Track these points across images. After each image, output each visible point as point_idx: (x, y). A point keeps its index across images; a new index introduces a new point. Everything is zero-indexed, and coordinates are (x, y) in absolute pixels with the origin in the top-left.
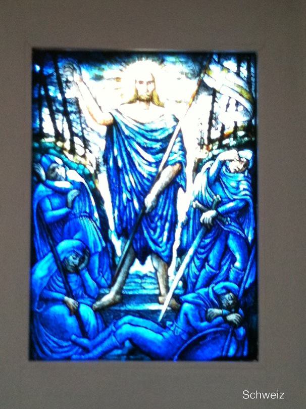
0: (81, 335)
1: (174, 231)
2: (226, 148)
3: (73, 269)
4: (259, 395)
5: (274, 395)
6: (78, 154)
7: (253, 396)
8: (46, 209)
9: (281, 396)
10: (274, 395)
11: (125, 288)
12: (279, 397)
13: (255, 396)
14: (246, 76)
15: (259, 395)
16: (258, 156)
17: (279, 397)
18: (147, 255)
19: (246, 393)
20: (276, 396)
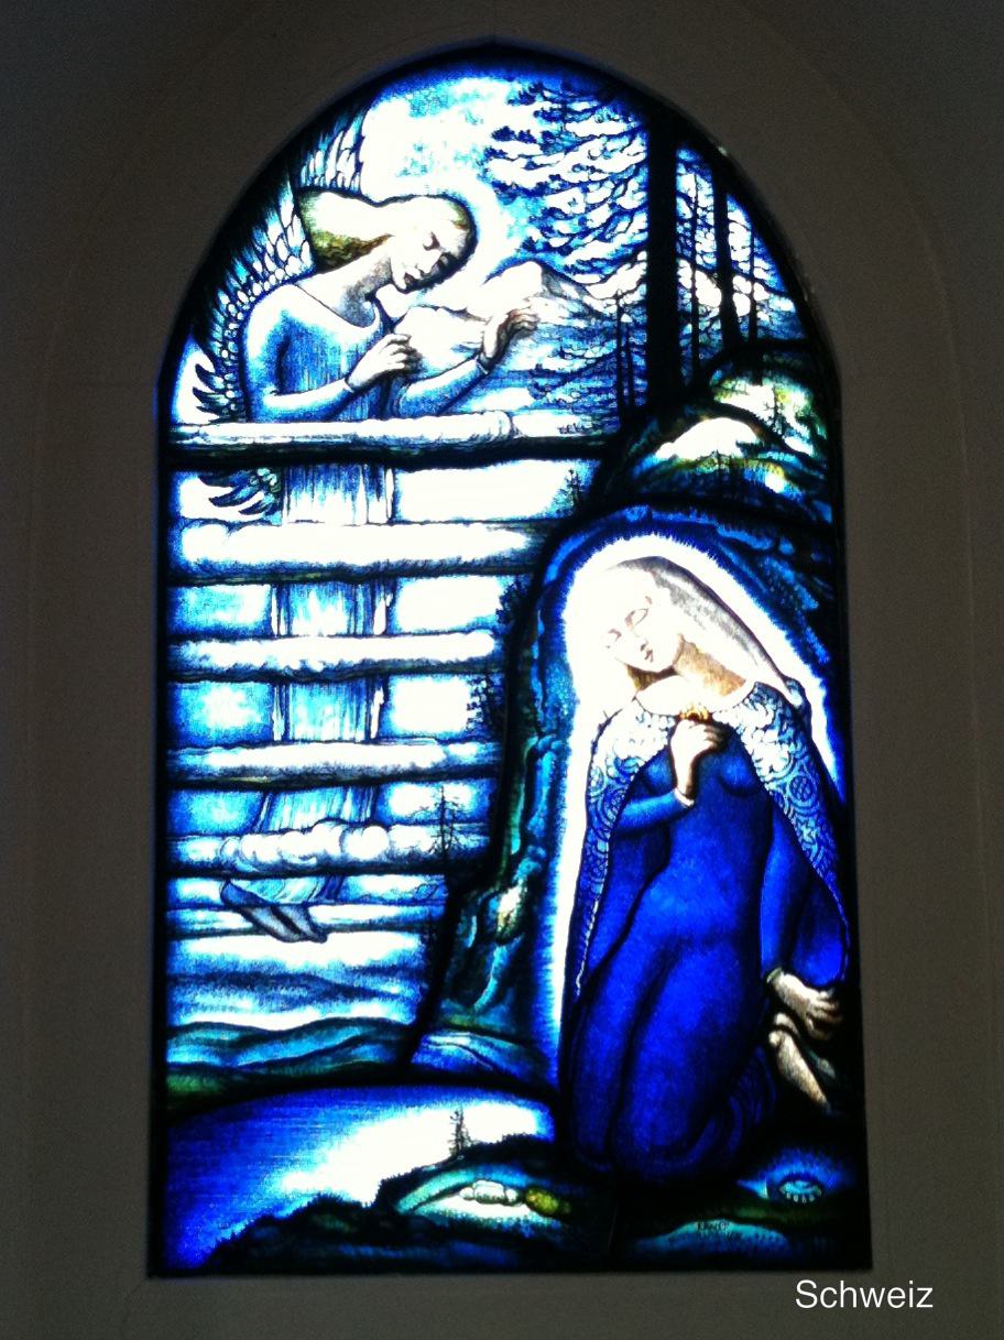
0: (316, 1218)
1: (405, 444)
2: (340, 996)
3: (506, 1061)
4: (848, 1295)
5: (893, 1301)
6: (740, 292)
7: (829, 1298)
8: (674, 807)
9: (921, 1298)
10: (894, 1301)
11: (592, 794)
12: (916, 1302)
13: (837, 1297)
14: (314, 879)
15: (848, 1295)
16: (154, 403)
17: (916, 1302)
18: (444, 874)
19: (806, 1287)
20: (907, 1299)
